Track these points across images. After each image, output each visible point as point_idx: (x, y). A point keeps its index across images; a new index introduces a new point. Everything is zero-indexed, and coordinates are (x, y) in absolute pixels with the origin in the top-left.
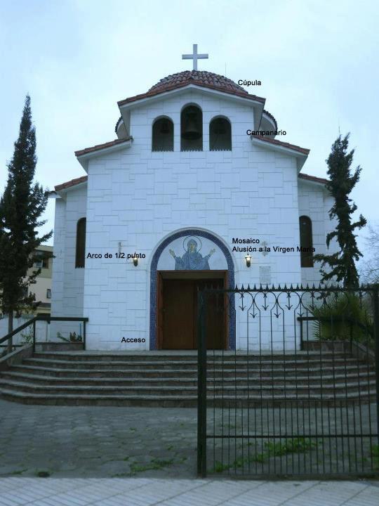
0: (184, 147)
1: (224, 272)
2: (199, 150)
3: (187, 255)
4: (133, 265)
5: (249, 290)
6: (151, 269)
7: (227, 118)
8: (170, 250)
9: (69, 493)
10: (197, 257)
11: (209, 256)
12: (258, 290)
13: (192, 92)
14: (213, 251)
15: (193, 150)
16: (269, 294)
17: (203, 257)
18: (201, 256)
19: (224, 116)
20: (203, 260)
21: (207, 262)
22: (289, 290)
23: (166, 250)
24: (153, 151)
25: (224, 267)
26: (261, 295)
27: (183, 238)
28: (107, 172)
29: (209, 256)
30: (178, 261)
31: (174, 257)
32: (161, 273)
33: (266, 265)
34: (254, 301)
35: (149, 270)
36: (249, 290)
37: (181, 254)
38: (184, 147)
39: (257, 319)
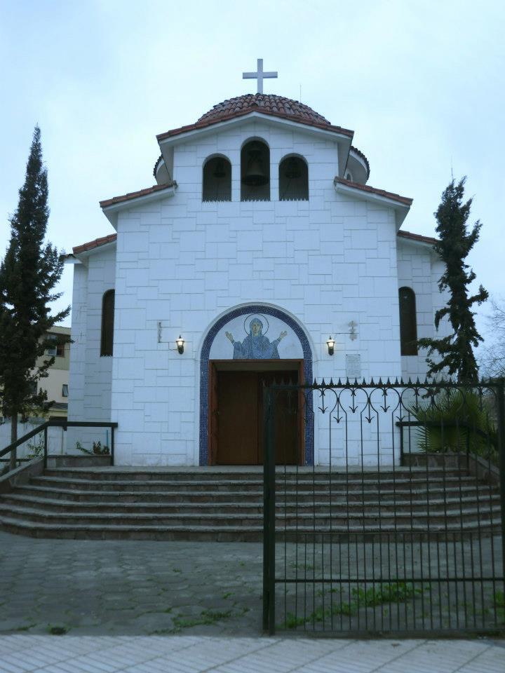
0: (246, 196)
1: (298, 362)
3: (249, 339)
5: (331, 386)
7: (302, 156)
10: (263, 342)
11: (279, 340)
12: (344, 386)
13: (256, 122)
14: (284, 334)
16: (358, 392)
17: (271, 341)
18: (268, 340)
22: (414, 385)
23: (221, 333)
25: (298, 354)
26: (348, 392)
27: (244, 317)
29: (279, 340)
30: (237, 347)
31: (233, 342)
32: (215, 363)
33: (355, 352)
35: (199, 359)
36: (331, 386)
37: (241, 337)
38: (246, 196)
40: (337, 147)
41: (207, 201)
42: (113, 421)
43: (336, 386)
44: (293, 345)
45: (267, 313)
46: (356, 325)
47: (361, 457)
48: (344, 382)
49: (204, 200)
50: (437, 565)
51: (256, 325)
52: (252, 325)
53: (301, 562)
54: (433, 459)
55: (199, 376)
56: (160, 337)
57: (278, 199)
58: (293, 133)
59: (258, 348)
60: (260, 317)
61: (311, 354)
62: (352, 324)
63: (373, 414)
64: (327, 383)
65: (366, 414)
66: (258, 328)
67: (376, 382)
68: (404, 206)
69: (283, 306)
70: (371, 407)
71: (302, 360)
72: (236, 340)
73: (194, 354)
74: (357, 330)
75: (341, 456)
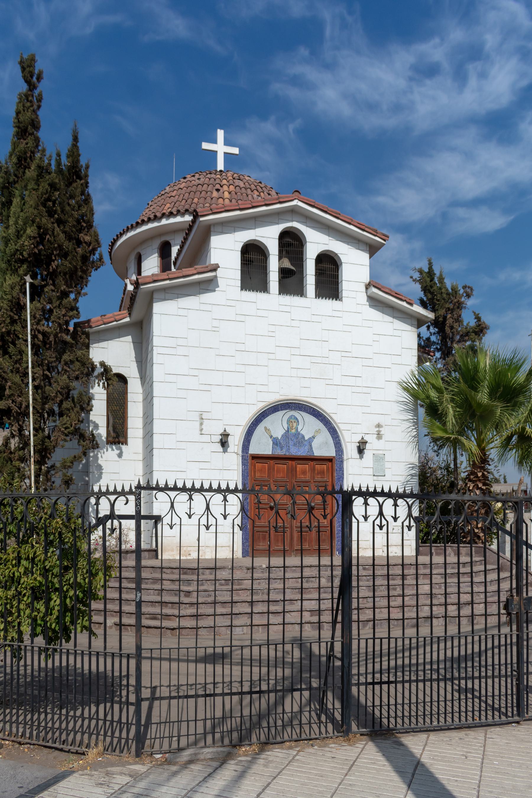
0: (284, 290)
1: (330, 460)
2: (264, 292)
3: (286, 435)
4: (219, 445)
5: (201, 490)
6: (243, 452)
7: (336, 254)
8: (266, 428)
9: (331, 746)
10: (299, 438)
11: (314, 437)
12: (215, 491)
13: (294, 212)
14: (318, 431)
15: (294, 295)
16: (197, 497)
17: (306, 438)
18: (303, 437)
19: (266, 247)
20: (305, 443)
21: (311, 446)
22: (224, 491)
23: (260, 428)
24: (280, 294)
25: (331, 452)
26: (184, 497)
27: (280, 413)
28: (181, 312)
29: (314, 437)
30: (276, 442)
31: (271, 437)
32: (256, 458)
33: (381, 452)
34: (208, 508)
35: (240, 453)
36: (201, 490)
37: (279, 433)
38: (284, 290)
39: (176, 528)
40: (368, 249)
41: (246, 290)
42: (155, 513)
43: (206, 491)
44: (326, 443)
45: (301, 411)
46: (382, 427)
47: (386, 548)
48: (180, 485)
49: (242, 289)
50: (391, 661)
51: (292, 420)
52: (289, 421)
53: (183, 681)
54: (451, 549)
55: (241, 470)
56: (201, 430)
57: (314, 297)
58: (328, 229)
59: (295, 445)
60: (296, 414)
61: (342, 452)
62: (379, 426)
63: (212, 521)
64: (198, 486)
65: (204, 521)
66: (295, 425)
67: (180, 485)
68: (173, 258)
69: (319, 404)
70: (209, 513)
71: (334, 457)
72: (274, 436)
73: (236, 447)
74: (383, 431)
75: (368, 547)
